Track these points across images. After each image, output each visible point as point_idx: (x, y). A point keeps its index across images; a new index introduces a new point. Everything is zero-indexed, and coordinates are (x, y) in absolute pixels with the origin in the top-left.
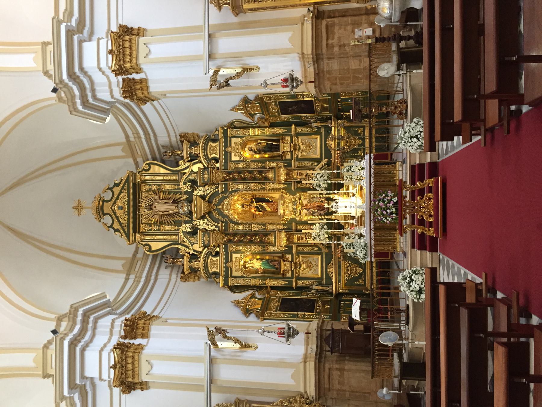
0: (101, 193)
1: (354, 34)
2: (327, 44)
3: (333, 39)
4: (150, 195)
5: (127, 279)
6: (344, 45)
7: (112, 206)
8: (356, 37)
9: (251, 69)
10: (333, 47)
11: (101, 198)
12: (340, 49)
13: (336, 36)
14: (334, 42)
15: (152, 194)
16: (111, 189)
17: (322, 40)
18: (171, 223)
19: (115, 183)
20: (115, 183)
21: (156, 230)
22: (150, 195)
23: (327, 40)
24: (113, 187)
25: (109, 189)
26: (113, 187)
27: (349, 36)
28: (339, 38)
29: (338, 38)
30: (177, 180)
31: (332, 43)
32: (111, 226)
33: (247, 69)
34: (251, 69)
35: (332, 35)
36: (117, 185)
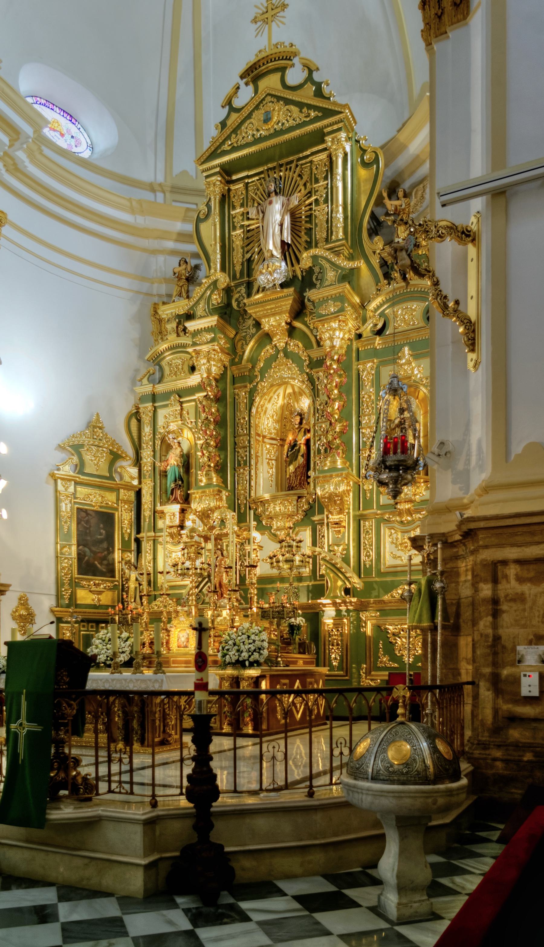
0: (302, 55)
1: (530, 643)
2: (504, 563)
3: (520, 580)
4: (305, 185)
5: (152, 188)
6: (496, 614)
7: (272, 96)
8: (520, 648)
9: (472, 345)
10: (495, 581)
11: (290, 59)
12: (484, 600)
13: (527, 589)
14: (508, 582)
15: (307, 191)
16: (310, 79)
17: (513, 545)
18: (248, 252)
19: (321, 83)
20: (321, 83)
21: (233, 222)
22: (305, 185)
23: (519, 562)
24: (314, 83)
25: (310, 72)
26: (314, 83)
27: (524, 626)
28: (520, 598)
29: (523, 594)
30: (331, 239)
31: (506, 577)
32: (232, 110)
33: (474, 339)
34: (473, 344)
35: (532, 574)
36: (319, 93)
